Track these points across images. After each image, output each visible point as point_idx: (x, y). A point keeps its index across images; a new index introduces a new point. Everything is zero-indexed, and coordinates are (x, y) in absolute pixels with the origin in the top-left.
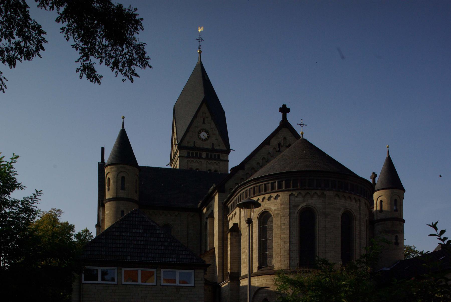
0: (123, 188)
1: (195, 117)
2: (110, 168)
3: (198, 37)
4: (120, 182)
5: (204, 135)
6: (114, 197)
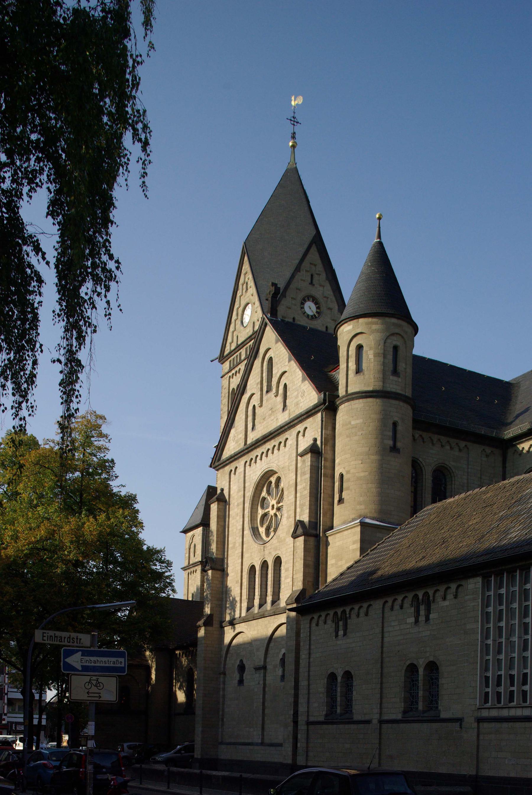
0: (395, 372)
1: (298, 269)
2: (367, 324)
3: (290, 116)
4: (390, 357)
5: (310, 308)
6: (378, 388)
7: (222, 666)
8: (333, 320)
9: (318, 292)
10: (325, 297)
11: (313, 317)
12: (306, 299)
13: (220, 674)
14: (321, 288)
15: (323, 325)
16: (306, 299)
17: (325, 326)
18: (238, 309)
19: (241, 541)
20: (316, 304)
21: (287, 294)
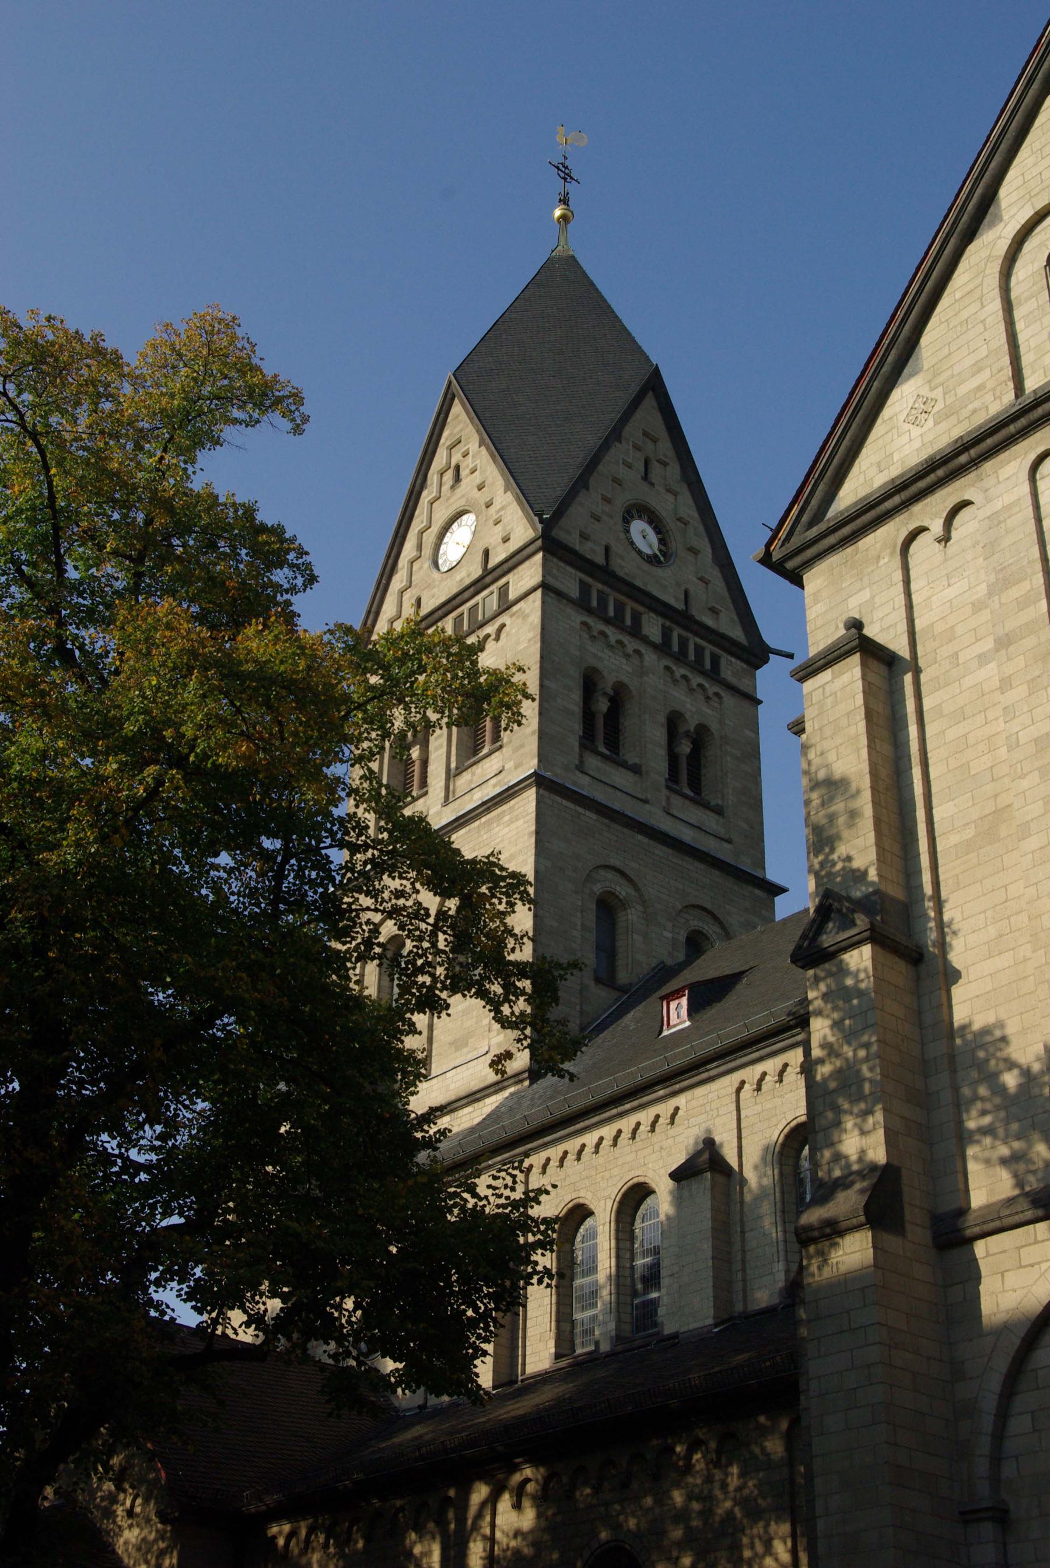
1: (615, 434)
7: (982, 1466)
8: (701, 579)
9: (663, 504)
10: (680, 520)
11: (652, 560)
12: (634, 512)
13: (969, 1517)
14: (670, 498)
15: (678, 584)
16: (634, 512)
17: (683, 588)
18: (421, 533)
19: (941, 870)
20: (658, 530)
21: (592, 481)
